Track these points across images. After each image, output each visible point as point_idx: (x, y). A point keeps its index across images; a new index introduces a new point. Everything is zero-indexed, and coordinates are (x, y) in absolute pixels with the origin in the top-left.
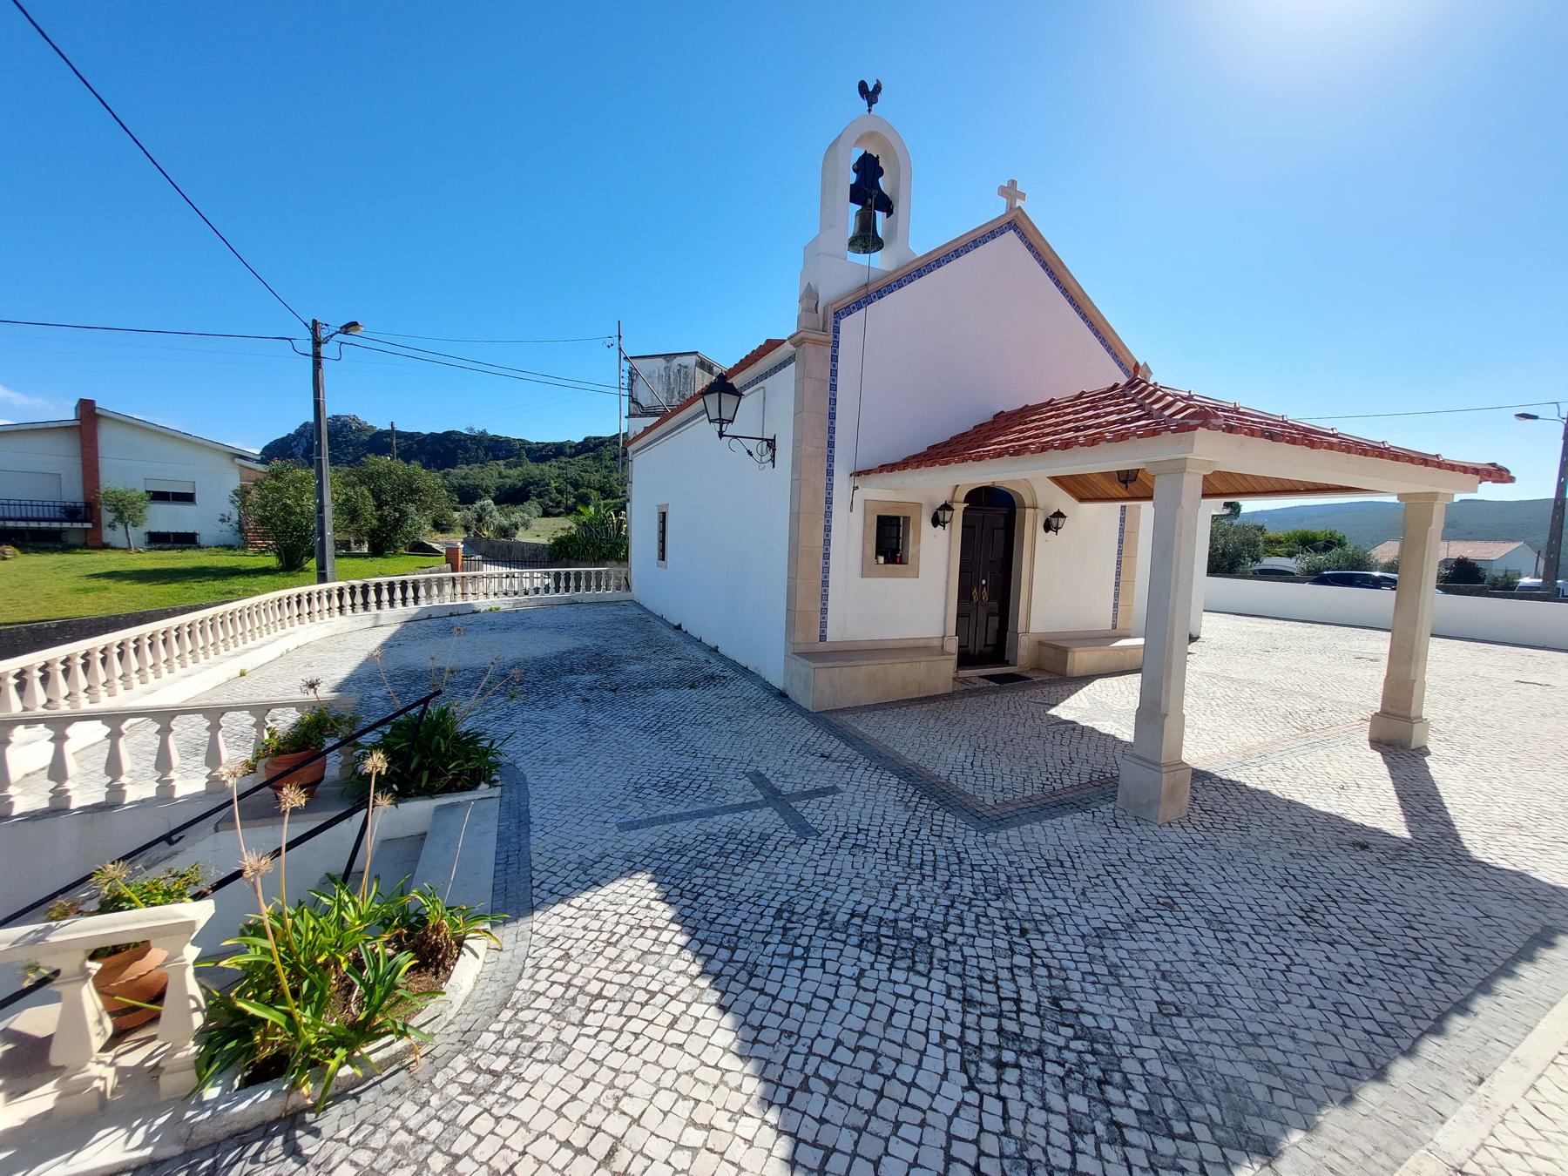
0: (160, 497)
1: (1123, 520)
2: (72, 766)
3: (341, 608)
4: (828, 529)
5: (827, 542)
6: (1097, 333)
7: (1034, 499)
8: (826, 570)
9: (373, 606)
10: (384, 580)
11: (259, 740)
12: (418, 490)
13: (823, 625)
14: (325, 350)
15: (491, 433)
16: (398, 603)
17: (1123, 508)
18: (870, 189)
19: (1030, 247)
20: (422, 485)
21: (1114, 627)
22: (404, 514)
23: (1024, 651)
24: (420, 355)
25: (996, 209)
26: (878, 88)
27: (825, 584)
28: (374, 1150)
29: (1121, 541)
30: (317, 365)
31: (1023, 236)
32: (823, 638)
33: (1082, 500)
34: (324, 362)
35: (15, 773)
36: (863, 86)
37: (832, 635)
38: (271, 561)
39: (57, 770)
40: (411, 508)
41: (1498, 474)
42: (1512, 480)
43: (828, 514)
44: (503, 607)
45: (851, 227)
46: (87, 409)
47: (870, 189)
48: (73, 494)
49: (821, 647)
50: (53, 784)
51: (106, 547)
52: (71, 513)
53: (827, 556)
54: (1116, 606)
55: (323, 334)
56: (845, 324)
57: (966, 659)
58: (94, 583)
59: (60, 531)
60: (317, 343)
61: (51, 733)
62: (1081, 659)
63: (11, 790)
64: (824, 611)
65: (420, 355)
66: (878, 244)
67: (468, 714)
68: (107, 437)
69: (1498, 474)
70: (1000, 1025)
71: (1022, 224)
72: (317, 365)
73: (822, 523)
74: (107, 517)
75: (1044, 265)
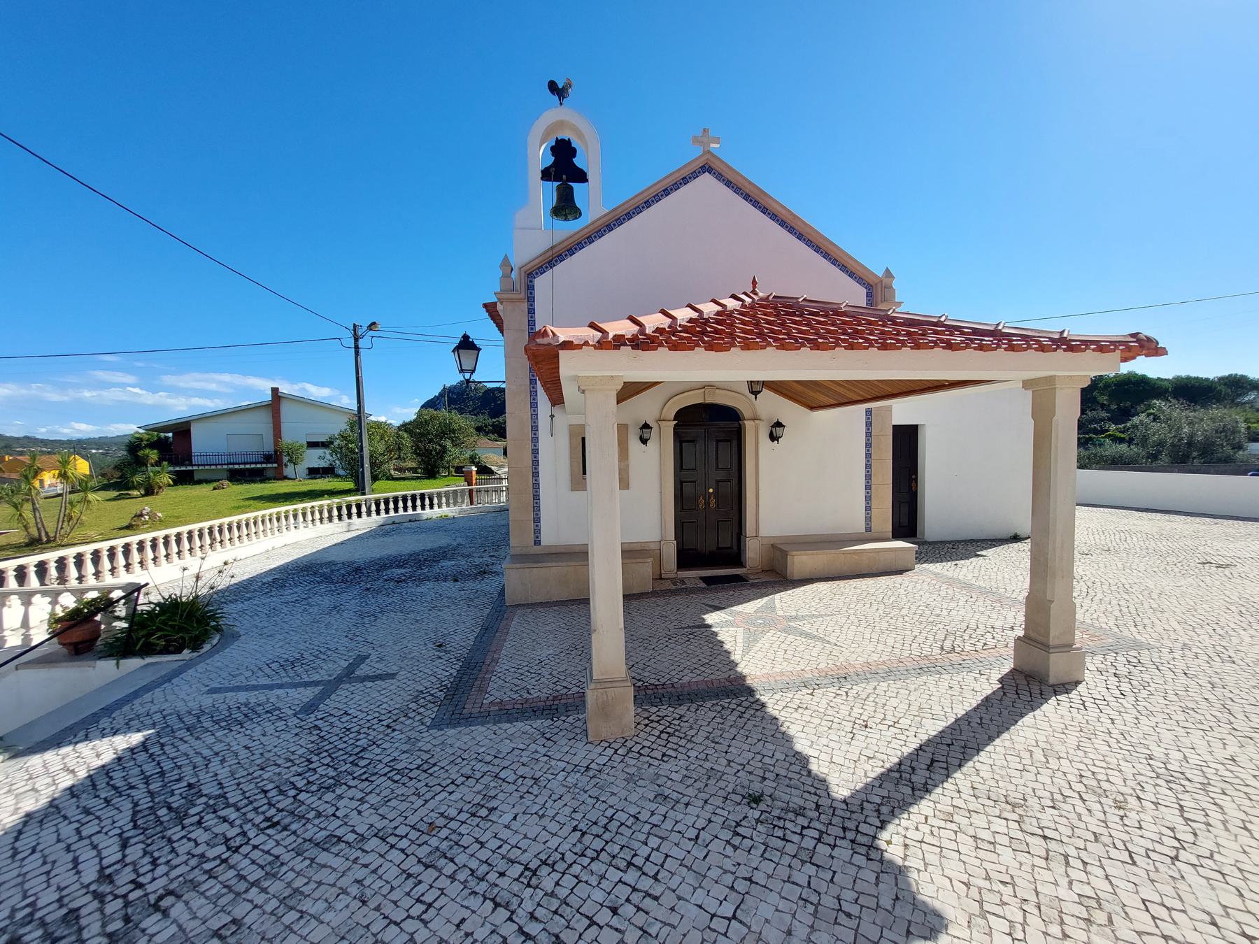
0: (312, 445)
1: (869, 424)
2: (32, 623)
3: (313, 520)
4: (535, 452)
5: (535, 463)
6: (817, 249)
7: (754, 411)
8: (536, 486)
9: (345, 517)
10: (418, 492)
11: (52, 614)
12: (453, 431)
13: (537, 532)
14: (361, 343)
15: (448, 386)
16: (374, 514)
17: (869, 412)
18: (564, 167)
19: (728, 183)
20: (456, 427)
21: (868, 529)
22: (444, 450)
23: (753, 552)
24: (435, 339)
25: (690, 155)
26: (569, 84)
27: (536, 497)
28: (421, 902)
29: (868, 445)
30: (357, 354)
31: (719, 176)
32: (537, 542)
33: (812, 408)
34: (361, 351)
35: (6, 625)
36: (553, 86)
37: (547, 538)
38: (350, 485)
39: (25, 623)
40: (448, 443)
41: (1149, 347)
42: (1166, 353)
43: (535, 440)
44: (451, 515)
45: (553, 200)
46: (275, 391)
47: (564, 167)
48: (269, 447)
49: (537, 549)
50: (23, 631)
51: (286, 478)
52: (268, 458)
53: (536, 474)
54: (868, 509)
55: (360, 332)
56: (541, 283)
57: (686, 558)
58: (247, 503)
59: (264, 469)
60: (356, 339)
61: (49, 599)
62: (800, 562)
63: (5, 633)
64: (537, 520)
65: (435, 339)
66: (577, 213)
67: (703, 585)
68: (286, 409)
69: (1149, 347)
70: (246, 880)
71: (716, 165)
72: (357, 354)
73: (529, 447)
74: (286, 459)
75: (747, 197)
